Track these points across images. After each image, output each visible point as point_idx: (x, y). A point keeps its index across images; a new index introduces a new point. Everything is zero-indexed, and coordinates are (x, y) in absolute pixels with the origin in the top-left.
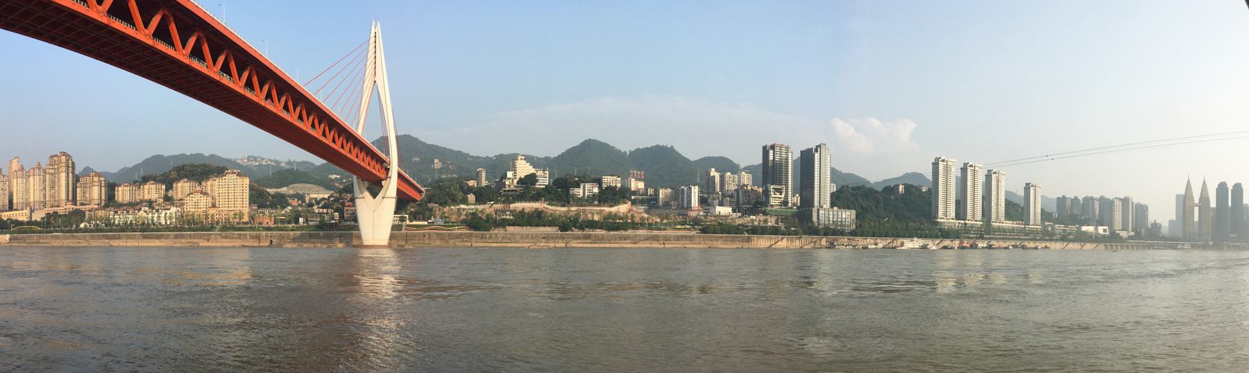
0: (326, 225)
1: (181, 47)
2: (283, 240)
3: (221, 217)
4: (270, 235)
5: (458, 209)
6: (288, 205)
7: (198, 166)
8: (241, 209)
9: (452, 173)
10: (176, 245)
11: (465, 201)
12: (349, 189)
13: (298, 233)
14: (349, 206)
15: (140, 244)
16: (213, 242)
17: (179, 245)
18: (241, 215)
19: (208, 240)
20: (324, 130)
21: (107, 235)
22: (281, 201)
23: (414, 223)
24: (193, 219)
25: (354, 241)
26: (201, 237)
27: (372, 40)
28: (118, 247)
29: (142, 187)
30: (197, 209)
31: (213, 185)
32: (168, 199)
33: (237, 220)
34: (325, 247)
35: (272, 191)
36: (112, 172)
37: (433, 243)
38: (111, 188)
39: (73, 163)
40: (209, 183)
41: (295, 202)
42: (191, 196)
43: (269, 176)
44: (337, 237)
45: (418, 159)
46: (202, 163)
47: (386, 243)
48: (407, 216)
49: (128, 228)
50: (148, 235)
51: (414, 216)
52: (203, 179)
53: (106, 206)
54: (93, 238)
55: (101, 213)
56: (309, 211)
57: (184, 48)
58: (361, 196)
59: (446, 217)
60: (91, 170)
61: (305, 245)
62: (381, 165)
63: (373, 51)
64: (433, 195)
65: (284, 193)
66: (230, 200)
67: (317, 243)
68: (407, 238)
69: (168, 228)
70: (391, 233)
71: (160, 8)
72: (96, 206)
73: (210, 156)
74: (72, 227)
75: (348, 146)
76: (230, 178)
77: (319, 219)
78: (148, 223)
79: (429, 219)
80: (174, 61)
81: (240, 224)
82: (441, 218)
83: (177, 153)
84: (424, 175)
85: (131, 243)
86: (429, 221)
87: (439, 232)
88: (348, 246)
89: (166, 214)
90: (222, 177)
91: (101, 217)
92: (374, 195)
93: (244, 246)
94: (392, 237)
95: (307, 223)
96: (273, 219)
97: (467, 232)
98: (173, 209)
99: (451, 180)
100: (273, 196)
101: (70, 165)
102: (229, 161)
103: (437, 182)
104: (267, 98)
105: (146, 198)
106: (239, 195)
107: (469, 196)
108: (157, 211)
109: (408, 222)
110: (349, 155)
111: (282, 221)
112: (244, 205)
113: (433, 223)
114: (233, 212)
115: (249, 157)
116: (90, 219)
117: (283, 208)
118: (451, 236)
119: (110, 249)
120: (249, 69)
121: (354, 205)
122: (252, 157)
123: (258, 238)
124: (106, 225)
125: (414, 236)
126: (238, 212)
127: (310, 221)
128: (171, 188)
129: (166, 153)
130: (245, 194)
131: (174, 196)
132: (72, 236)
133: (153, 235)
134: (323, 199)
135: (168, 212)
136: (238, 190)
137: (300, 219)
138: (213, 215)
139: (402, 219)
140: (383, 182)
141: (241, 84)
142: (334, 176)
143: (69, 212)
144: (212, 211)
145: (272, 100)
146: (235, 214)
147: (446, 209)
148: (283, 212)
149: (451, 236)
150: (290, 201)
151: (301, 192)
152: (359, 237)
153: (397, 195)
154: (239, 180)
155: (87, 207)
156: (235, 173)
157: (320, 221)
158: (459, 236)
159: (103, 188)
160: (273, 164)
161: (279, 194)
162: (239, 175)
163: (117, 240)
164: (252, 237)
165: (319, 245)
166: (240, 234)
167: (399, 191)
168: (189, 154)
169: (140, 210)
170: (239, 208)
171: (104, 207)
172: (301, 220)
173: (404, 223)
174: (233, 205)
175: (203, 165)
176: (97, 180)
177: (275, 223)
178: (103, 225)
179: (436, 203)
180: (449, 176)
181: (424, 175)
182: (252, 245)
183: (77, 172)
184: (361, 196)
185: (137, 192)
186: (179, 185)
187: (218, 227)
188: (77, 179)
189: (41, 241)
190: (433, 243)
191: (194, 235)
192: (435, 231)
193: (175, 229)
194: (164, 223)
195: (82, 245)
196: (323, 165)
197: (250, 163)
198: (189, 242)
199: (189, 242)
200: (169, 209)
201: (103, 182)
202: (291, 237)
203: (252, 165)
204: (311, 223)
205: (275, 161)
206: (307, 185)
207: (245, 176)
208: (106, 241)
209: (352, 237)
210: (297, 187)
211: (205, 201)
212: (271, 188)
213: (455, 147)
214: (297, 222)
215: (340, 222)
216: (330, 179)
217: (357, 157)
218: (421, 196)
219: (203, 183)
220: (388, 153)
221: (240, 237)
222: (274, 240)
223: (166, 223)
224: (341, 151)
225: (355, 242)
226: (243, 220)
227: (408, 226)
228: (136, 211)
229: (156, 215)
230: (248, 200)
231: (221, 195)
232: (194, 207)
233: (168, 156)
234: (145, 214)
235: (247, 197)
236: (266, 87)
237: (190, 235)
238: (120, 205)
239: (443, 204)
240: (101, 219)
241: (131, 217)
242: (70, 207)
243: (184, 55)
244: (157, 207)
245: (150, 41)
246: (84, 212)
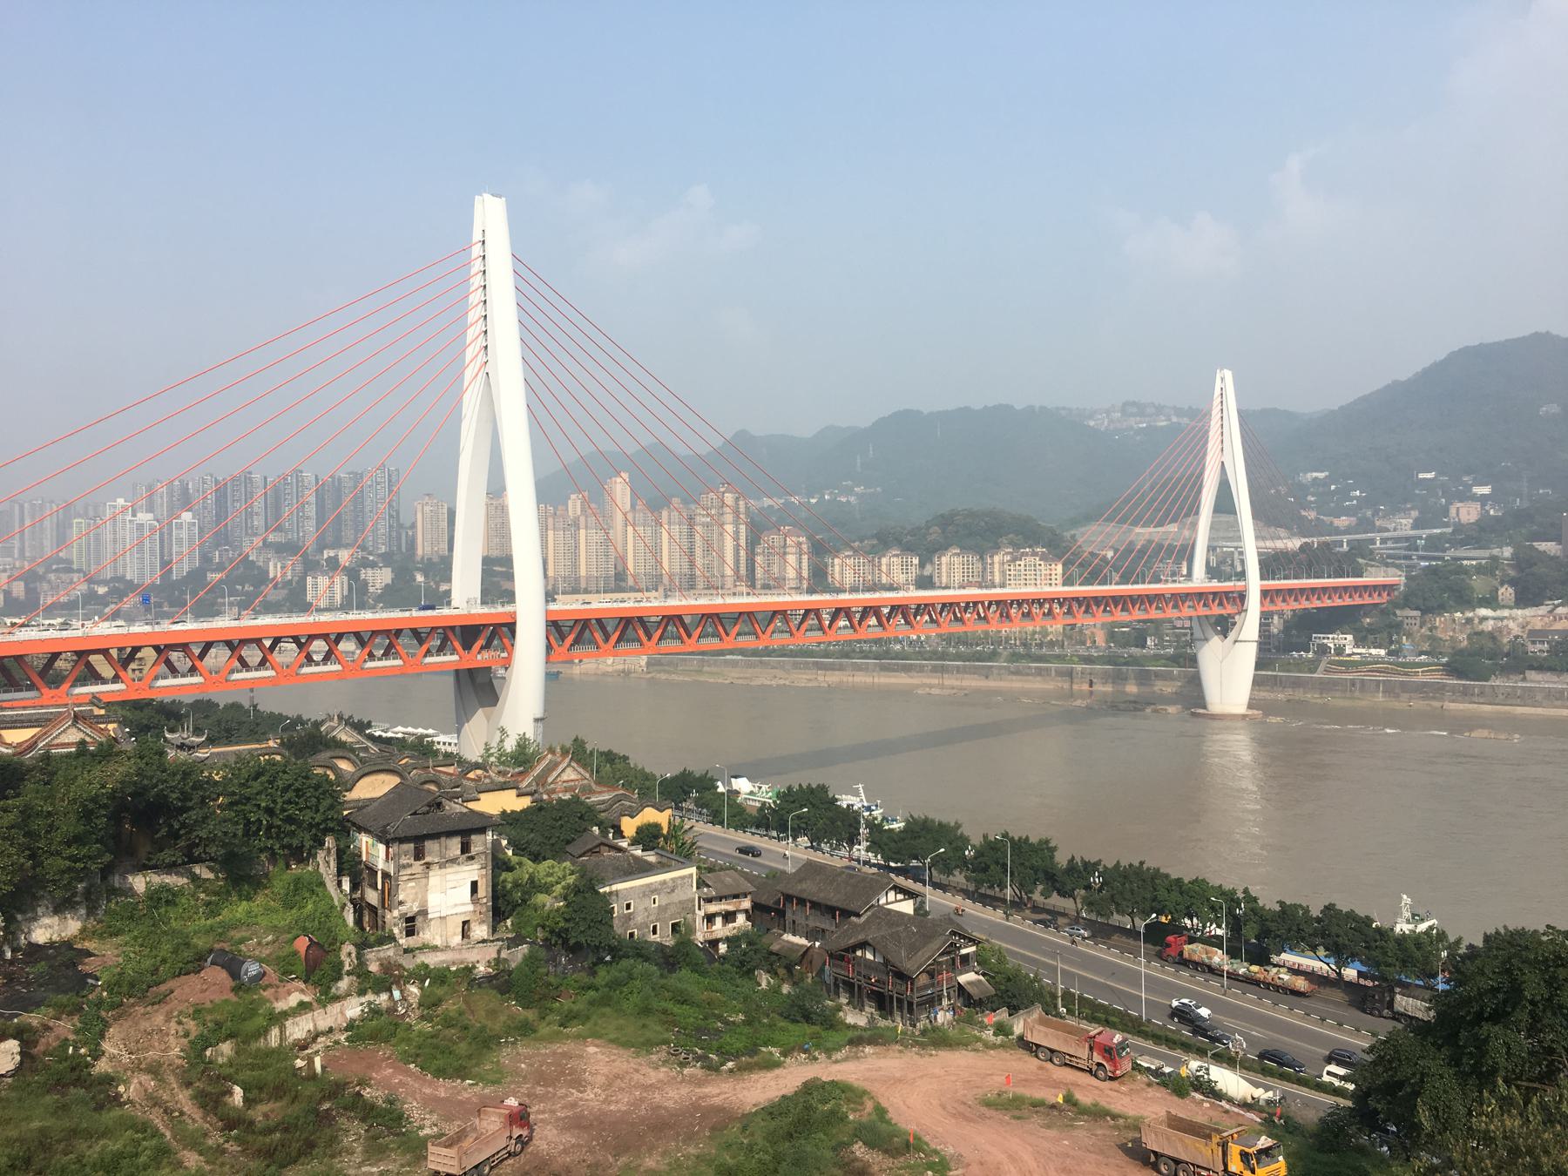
4: (1088, 671)
16: (995, 680)
19: (987, 677)
85: (861, 679)
115: (1125, 404)
122: (1134, 404)
123: (1070, 674)
132: (761, 662)
133: (898, 664)
153: (1260, 636)
163: (837, 673)
164: (1060, 673)
168: (978, 406)
179: (1417, 609)
189: (706, 669)
191: (965, 666)
221: (1039, 672)
237: (958, 667)
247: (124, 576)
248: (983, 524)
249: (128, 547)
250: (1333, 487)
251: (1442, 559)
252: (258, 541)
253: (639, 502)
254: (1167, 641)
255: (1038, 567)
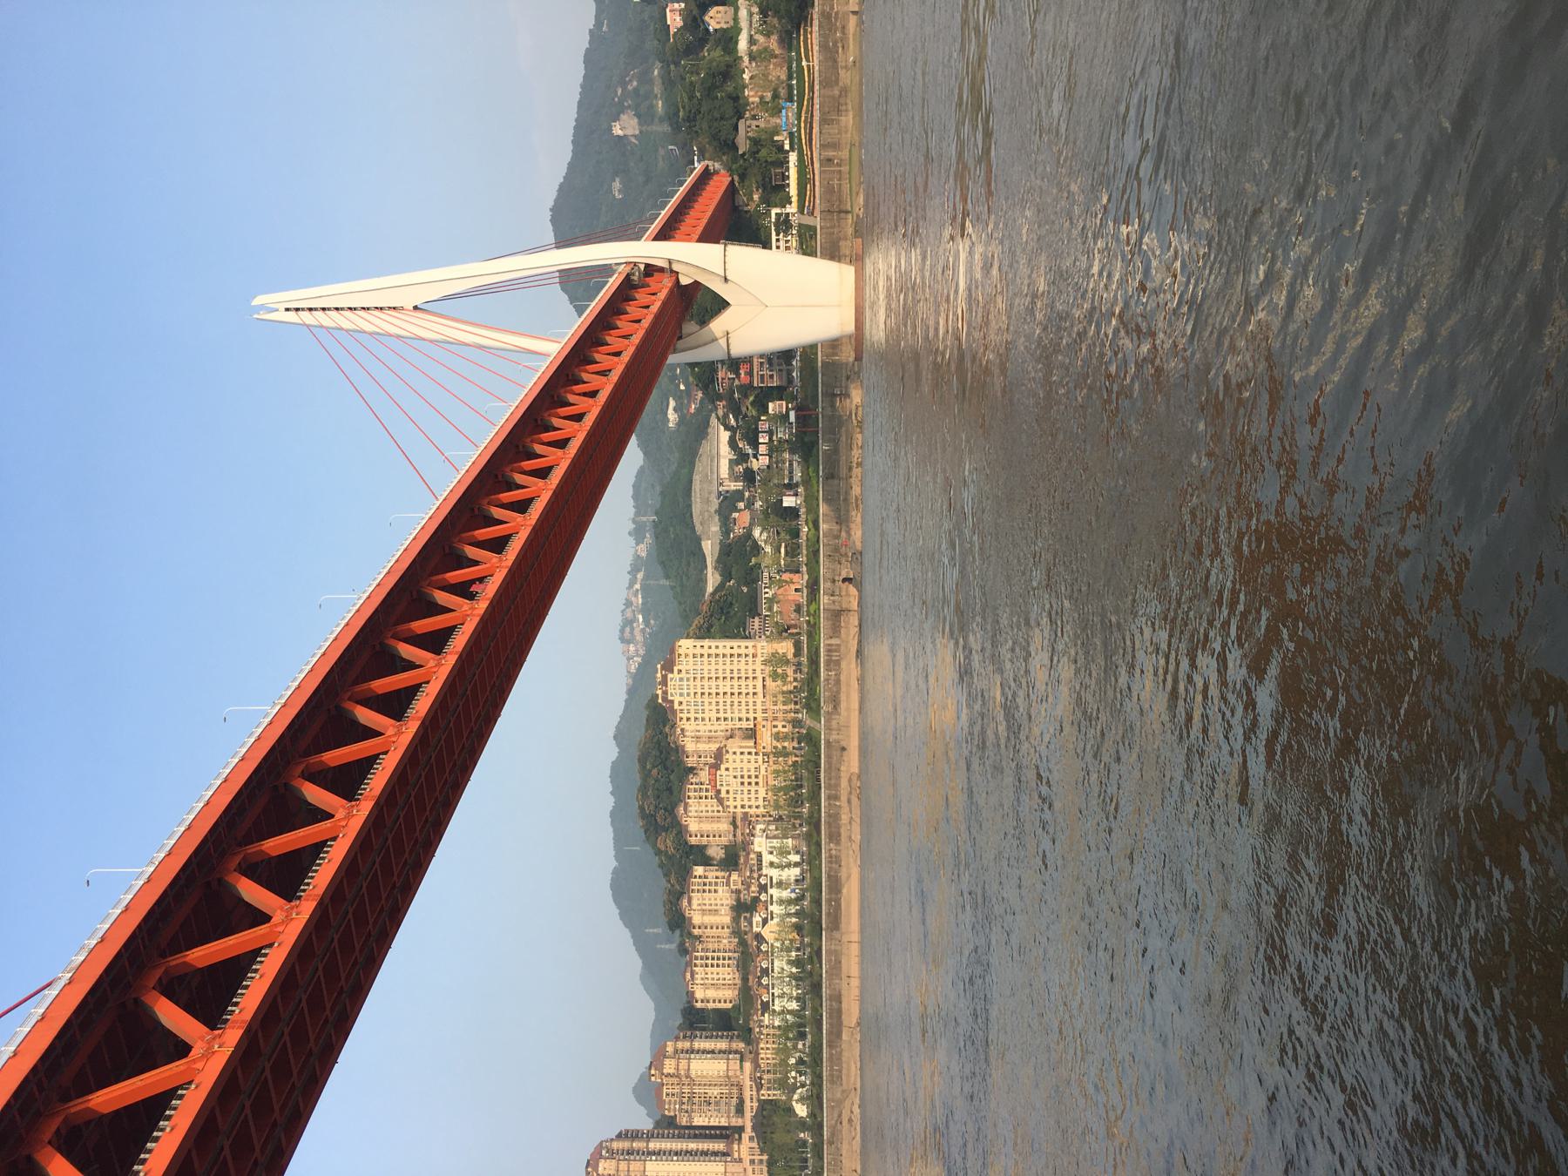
0: (801, 434)
1: (327, 824)
2: (843, 550)
3: (780, 715)
4: (829, 584)
5: (752, 58)
6: (748, 535)
7: (646, 777)
8: (759, 659)
9: (651, 82)
10: (857, 837)
11: (728, 38)
12: (705, 374)
13: (823, 508)
14: (750, 374)
15: (855, 937)
16: (849, 736)
17: (856, 828)
18: (775, 660)
19: (844, 749)
20: (550, 444)
21: (830, 1033)
22: (738, 555)
23: (793, 190)
24: (785, 789)
25: (844, 359)
26: (834, 770)
27: (306, 317)
28: (862, 1000)
29: (696, 932)
30: (760, 780)
31: (695, 734)
32: (732, 859)
33: (790, 671)
34: (859, 436)
35: (712, 580)
36: (652, 1016)
37: (850, 135)
38: (697, 1021)
39: (619, 1136)
40: (690, 746)
41: (742, 518)
42: (723, 794)
43: (673, 588)
44: (833, 406)
45: (617, 185)
46: (637, 767)
47: (849, 271)
48: (774, 211)
49: (811, 974)
50: (828, 914)
51: (775, 191)
52: (680, 763)
53: (747, 1035)
54: (836, 1078)
55: (767, 1052)
56: (765, 482)
57: (333, 816)
58: (723, 342)
59: (776, 96)
60: (645, 1078)
61: (856, 490)
62: (635, 287)
63: (334, 314)
64: (715, 137)
65: (717, 548)
66: (736, 691)
67: (849, 456)
68: (835, 210)
69: (811, 860)
70: (823, 256)
71: (220, 880)
72: (748, 1066)
73: (618, 745)
74: (804, 1143)
75: (590, 379)
76: (679, 690)
77: (787, 455)
78: (797, 914)
79: (780, 148)
80: (363, 843)
81: (799, 664)
82: (777, 111)
83: (608, 834)
84: (661, 163)
85: (852, 964)
86: (787, 147)
87: (816, 118)
88: (858, 374)
89: (772, 864)
90: (674, 712)
91: (777, 1051)
92: (721, 305)
93: (859, 653)
94: (833, 254)
95: (797, 485)
96: (786, 576)
97: (816, 28)
98: (760, 844)
99: (668, 83)
100: (726, 574)
101: (626, 1145)
102: (632, 692)
103: (676, 128)
104: (471, 596)
105: (727, 920)
106: (724, 667)
107: (713, 25)
108: (763, 888)
109: (792, 209)
110: (615, 376)
111: (793, 551)
112: (751, 651)
113: (791, 135)
114: (769, 682)
115: (623, 640)
116: (782, 1084)
117: (756, 549)
118: (829, 81)
119: (873, 1029)
120: (392, 642)
121: (748, 360)
122: (622, 631)
123: (837, 615)
124: (802, 1036)
125: (829, 190)
126: (768, 669)
127: (791, 478)
128: (701, 849)
129: (606, 861)
130: (721, 651)
131: (724, 841)
132: (831, 1143)
133: (829, 901)
134: (732, 443)
135: (767, 858)
136: (708, 667)
137: (785, 504)
138: (777, 737)
139: (784, 224)
140: (684, 281)
141: (432, 663)
142: (672, 416)
143: (762, 1152)
144: (766, 739)
145: (473, 582)
146: (775, 676)
147: (751, 95)
148: (768, 549)
149: (829, 81)
150: (738, 531)
151: (715, 504)
152: (834, 344)
153: (718, 242)
154: (684, 664)
155: (747, 1094)
156: (665, 678)
157: (792, 452)
158: (830, 53)
159: (696, 1045)
160: (640, 576)
161: (718, 561)
162: (669, 666)
163: (844, 1006)
164: (835, 630)
165: (856, 453)
166: (828, 663)
167: (707, 237)
168: (610, 802)
169: (759, 938)
170: (759, 667)
171: (748, 1042)
172: (789, 501)
173: (794, 220)
174: (750, 683)
175: (642, 760)
176: (673, 1062)
177: (798, 572)
178: (800, 1046)
179: (736, 128)
180: (657, 89)
181: (661, 163)
182: (854, 630)
183: (647, 1124)
184: (723, 342)
185: (710, 946)
186: (693, 826)
187: (809, 722)
188: (668, 1125)
190: (850, 135)
191: (828, 787)
192: (816, 130)
193: (813, 839)
194: (797, 871)
195: (857, 1110)
196: (643, 446)
197: (639, 638)
198: (849, 801)
199: (849, 801)
200: (759, 855)
201: (680, 1045)
202: (836, 527)
203: (643, 631)
204: (798, 475)
205: (634, 570)
206: (696, 486)
207: (673, 651)
208: (845, 1037)
209: (834, 363)
210: (702, 513)
211: (738, 757)
212: (702, 581)
213: (575, 73)
214: (793, 512)
215: (792, 398)
216: (678, 424)
217: (618, 354)
218: (716, 172)
219: (691, 761)
220: (606, 270)
221: (834, 664)
222: (844, 575)
223: (796, 865)
224: (603, 396)
225: (847, 355)
226: (790, 656)
227: (801, 210)
228: (764, 948)
229: (775, 892)
230: (735, 643)
231: (721, 715)
232: (753, 788)
233: (616, 857)
234: (773, 924)
235: (729, 643)
236: (442, 597)
237: (829, 798)
238: (746, 994)
239: (738, 107)
240: (784, 1052)
241: (779, 964)
242: (746, 1147)
243: (349, 816)
244: (753, 888)
245: (306, 908)
246: (764, 1105)
248: (655, 771)
250: (682, 387)
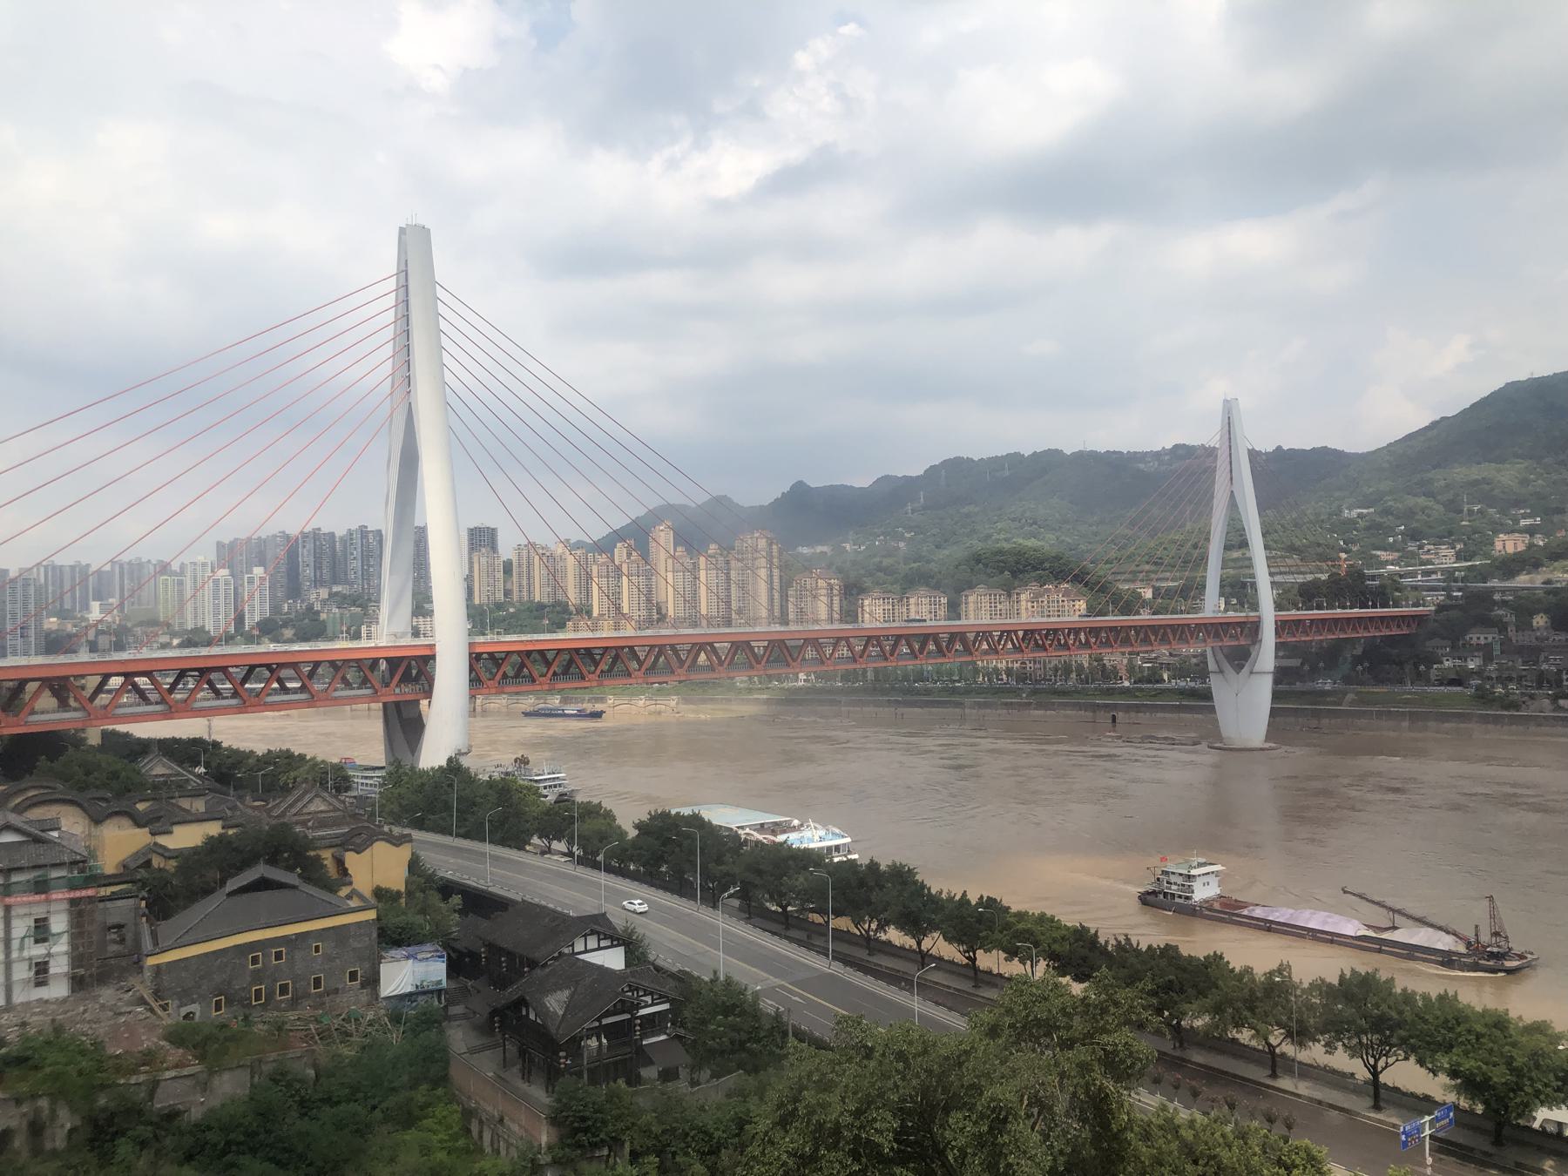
168: (1027, 452)
247: (204, 626)
249: (50, 601)
251: (1381, 576)
252: (324, 593)
253: (634, 553)
254: (983, 679)
255: (1061, 604)
